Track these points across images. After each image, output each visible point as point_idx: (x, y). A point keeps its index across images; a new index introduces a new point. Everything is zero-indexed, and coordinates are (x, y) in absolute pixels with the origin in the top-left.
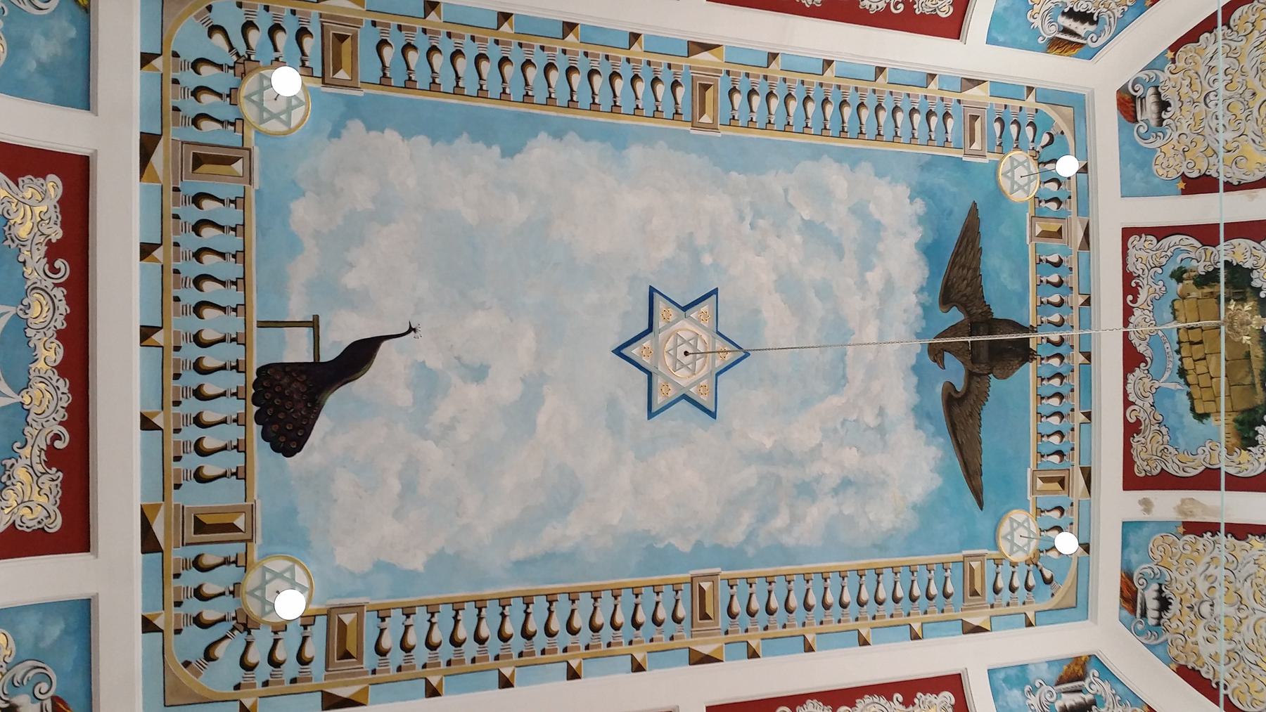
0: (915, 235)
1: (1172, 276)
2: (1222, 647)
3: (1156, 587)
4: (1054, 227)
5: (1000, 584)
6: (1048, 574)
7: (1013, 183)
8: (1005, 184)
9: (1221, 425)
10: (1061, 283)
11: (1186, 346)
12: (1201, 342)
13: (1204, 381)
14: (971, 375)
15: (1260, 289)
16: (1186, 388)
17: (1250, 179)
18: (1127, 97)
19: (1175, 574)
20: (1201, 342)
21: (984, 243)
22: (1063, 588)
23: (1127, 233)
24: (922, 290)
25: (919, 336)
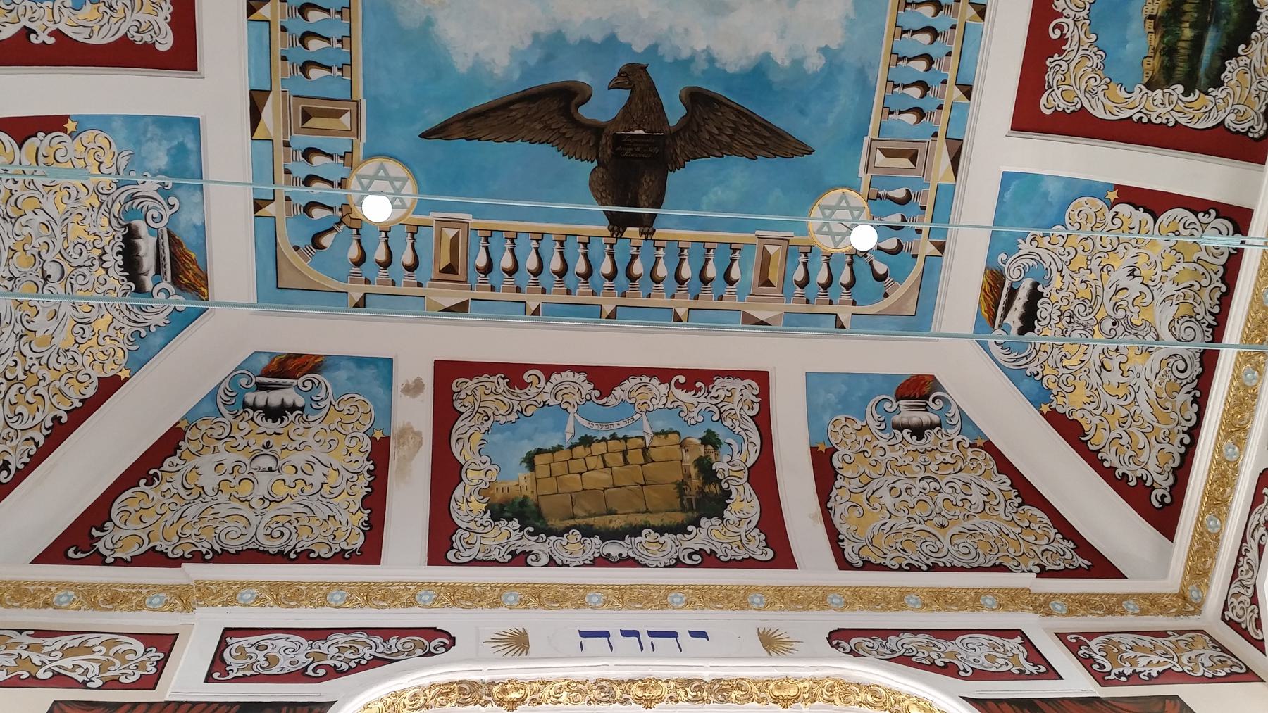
0: (781, 56)
1: (709, 432)
2: (209, 480)
3: (300, 402)
4: (774, 275)
5: (317, 160)
6: (327, 241)
7: (834, 209)
8: (832, 197)
9: (517, 480)
10: (705, 282)
11: (621, 445)
12: (626, 463)
13: (577, 465)
14: (597, 130)
15: (698, 526)
16: (567, 445)
17: (836, 520)
18: (927, 390)
19: (316, 427)
20: (626, 463)
21: (762, 163)
22: (305, 267)
23: (762, 378)
24: (711, 60)
25: (653, 48)
